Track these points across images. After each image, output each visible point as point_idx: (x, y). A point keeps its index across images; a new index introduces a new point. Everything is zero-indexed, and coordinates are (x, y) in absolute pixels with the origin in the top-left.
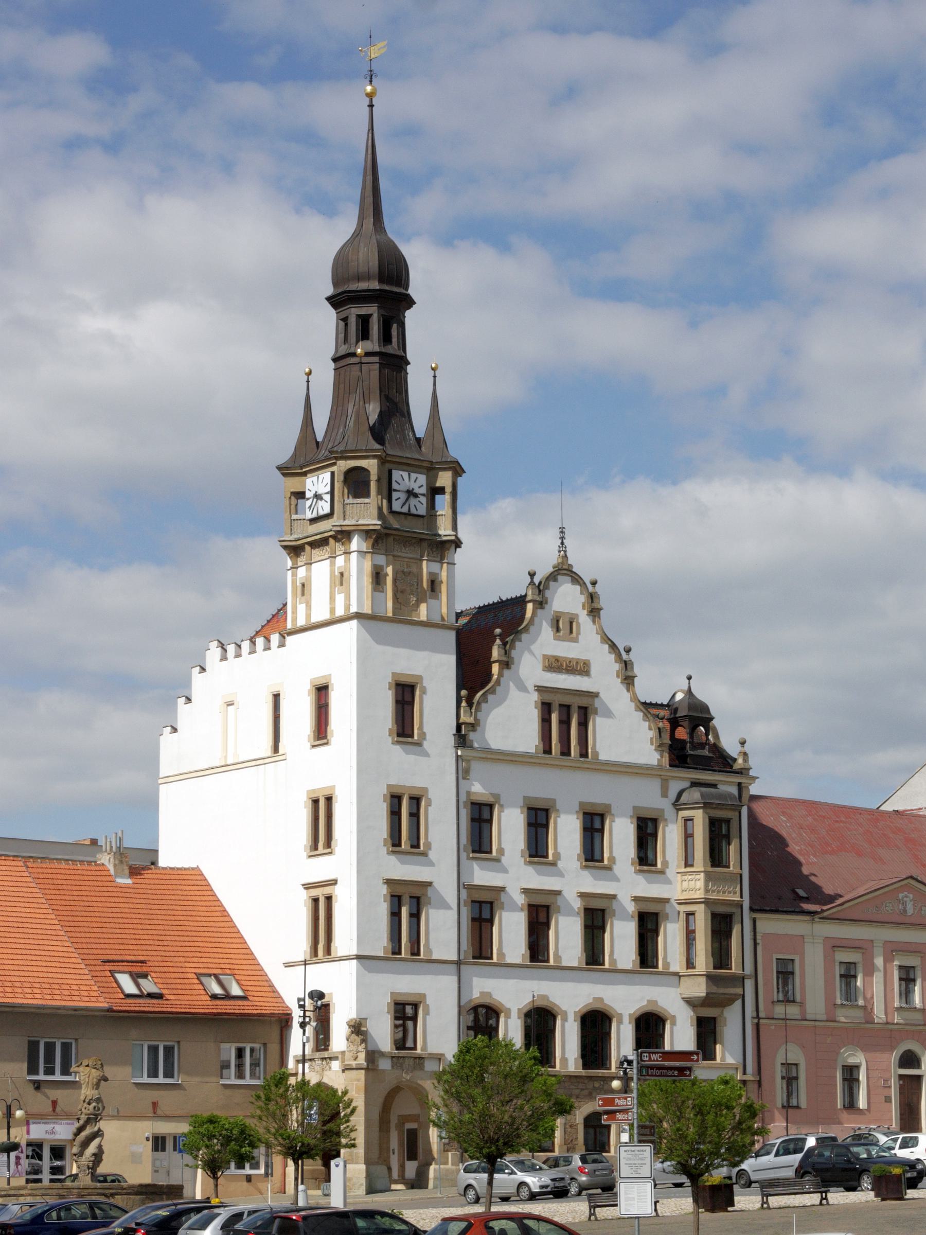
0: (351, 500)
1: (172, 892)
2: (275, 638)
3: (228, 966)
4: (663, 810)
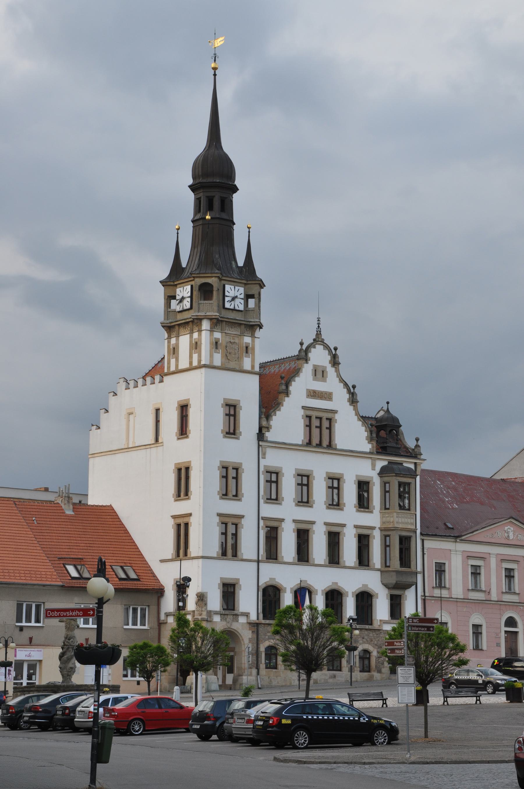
0: (202, 302)
1: (97, 519)
2: (157, 378)
3: (128, 562)
4: (372, 477)
